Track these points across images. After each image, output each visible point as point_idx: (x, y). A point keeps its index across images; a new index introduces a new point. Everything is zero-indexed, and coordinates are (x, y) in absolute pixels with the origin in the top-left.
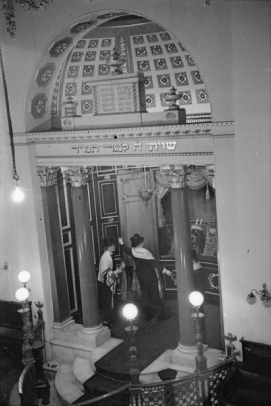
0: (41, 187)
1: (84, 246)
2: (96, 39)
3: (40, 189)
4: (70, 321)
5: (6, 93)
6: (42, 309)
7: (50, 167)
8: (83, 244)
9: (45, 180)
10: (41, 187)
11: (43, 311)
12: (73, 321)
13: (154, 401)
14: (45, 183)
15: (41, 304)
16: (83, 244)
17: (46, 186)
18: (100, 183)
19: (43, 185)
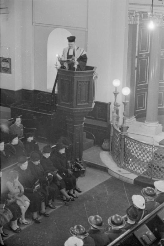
0: (129, 25)
1: (155, 71)
2: (144, 92)
3: (128, 26)
4: (89, 64)
5: (133, 134)
6: (118, 108)
7: (137, 11)
8: (155, 70)
9: (133, 20)
10: (129, 25)
11: (119, 109)
12: (135, 119)
13: (143, 152)
14: (133, 22)
15: (119, 104)
16: (155, 70)
17: (133, 24)
18: (144, 108)
19: (130, 23)
